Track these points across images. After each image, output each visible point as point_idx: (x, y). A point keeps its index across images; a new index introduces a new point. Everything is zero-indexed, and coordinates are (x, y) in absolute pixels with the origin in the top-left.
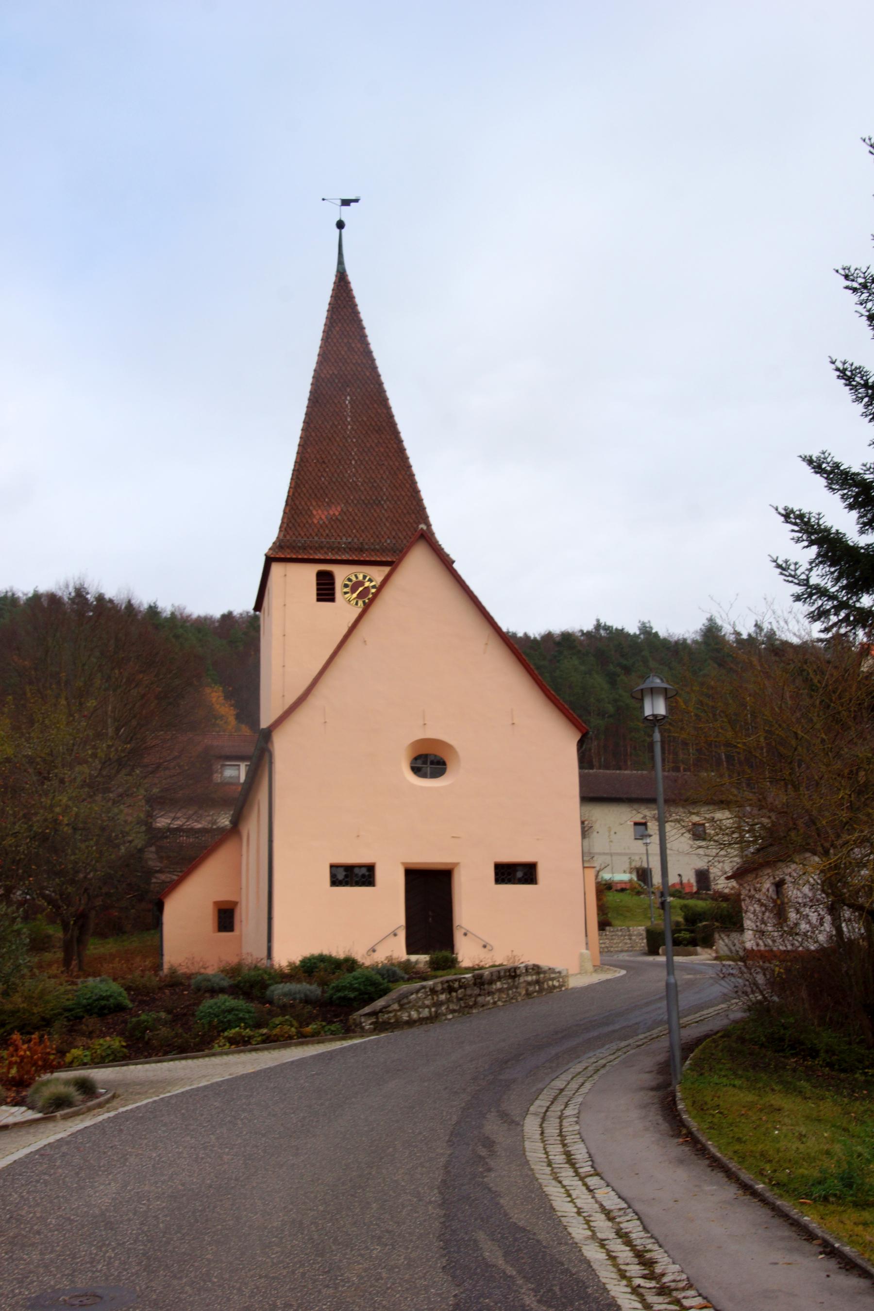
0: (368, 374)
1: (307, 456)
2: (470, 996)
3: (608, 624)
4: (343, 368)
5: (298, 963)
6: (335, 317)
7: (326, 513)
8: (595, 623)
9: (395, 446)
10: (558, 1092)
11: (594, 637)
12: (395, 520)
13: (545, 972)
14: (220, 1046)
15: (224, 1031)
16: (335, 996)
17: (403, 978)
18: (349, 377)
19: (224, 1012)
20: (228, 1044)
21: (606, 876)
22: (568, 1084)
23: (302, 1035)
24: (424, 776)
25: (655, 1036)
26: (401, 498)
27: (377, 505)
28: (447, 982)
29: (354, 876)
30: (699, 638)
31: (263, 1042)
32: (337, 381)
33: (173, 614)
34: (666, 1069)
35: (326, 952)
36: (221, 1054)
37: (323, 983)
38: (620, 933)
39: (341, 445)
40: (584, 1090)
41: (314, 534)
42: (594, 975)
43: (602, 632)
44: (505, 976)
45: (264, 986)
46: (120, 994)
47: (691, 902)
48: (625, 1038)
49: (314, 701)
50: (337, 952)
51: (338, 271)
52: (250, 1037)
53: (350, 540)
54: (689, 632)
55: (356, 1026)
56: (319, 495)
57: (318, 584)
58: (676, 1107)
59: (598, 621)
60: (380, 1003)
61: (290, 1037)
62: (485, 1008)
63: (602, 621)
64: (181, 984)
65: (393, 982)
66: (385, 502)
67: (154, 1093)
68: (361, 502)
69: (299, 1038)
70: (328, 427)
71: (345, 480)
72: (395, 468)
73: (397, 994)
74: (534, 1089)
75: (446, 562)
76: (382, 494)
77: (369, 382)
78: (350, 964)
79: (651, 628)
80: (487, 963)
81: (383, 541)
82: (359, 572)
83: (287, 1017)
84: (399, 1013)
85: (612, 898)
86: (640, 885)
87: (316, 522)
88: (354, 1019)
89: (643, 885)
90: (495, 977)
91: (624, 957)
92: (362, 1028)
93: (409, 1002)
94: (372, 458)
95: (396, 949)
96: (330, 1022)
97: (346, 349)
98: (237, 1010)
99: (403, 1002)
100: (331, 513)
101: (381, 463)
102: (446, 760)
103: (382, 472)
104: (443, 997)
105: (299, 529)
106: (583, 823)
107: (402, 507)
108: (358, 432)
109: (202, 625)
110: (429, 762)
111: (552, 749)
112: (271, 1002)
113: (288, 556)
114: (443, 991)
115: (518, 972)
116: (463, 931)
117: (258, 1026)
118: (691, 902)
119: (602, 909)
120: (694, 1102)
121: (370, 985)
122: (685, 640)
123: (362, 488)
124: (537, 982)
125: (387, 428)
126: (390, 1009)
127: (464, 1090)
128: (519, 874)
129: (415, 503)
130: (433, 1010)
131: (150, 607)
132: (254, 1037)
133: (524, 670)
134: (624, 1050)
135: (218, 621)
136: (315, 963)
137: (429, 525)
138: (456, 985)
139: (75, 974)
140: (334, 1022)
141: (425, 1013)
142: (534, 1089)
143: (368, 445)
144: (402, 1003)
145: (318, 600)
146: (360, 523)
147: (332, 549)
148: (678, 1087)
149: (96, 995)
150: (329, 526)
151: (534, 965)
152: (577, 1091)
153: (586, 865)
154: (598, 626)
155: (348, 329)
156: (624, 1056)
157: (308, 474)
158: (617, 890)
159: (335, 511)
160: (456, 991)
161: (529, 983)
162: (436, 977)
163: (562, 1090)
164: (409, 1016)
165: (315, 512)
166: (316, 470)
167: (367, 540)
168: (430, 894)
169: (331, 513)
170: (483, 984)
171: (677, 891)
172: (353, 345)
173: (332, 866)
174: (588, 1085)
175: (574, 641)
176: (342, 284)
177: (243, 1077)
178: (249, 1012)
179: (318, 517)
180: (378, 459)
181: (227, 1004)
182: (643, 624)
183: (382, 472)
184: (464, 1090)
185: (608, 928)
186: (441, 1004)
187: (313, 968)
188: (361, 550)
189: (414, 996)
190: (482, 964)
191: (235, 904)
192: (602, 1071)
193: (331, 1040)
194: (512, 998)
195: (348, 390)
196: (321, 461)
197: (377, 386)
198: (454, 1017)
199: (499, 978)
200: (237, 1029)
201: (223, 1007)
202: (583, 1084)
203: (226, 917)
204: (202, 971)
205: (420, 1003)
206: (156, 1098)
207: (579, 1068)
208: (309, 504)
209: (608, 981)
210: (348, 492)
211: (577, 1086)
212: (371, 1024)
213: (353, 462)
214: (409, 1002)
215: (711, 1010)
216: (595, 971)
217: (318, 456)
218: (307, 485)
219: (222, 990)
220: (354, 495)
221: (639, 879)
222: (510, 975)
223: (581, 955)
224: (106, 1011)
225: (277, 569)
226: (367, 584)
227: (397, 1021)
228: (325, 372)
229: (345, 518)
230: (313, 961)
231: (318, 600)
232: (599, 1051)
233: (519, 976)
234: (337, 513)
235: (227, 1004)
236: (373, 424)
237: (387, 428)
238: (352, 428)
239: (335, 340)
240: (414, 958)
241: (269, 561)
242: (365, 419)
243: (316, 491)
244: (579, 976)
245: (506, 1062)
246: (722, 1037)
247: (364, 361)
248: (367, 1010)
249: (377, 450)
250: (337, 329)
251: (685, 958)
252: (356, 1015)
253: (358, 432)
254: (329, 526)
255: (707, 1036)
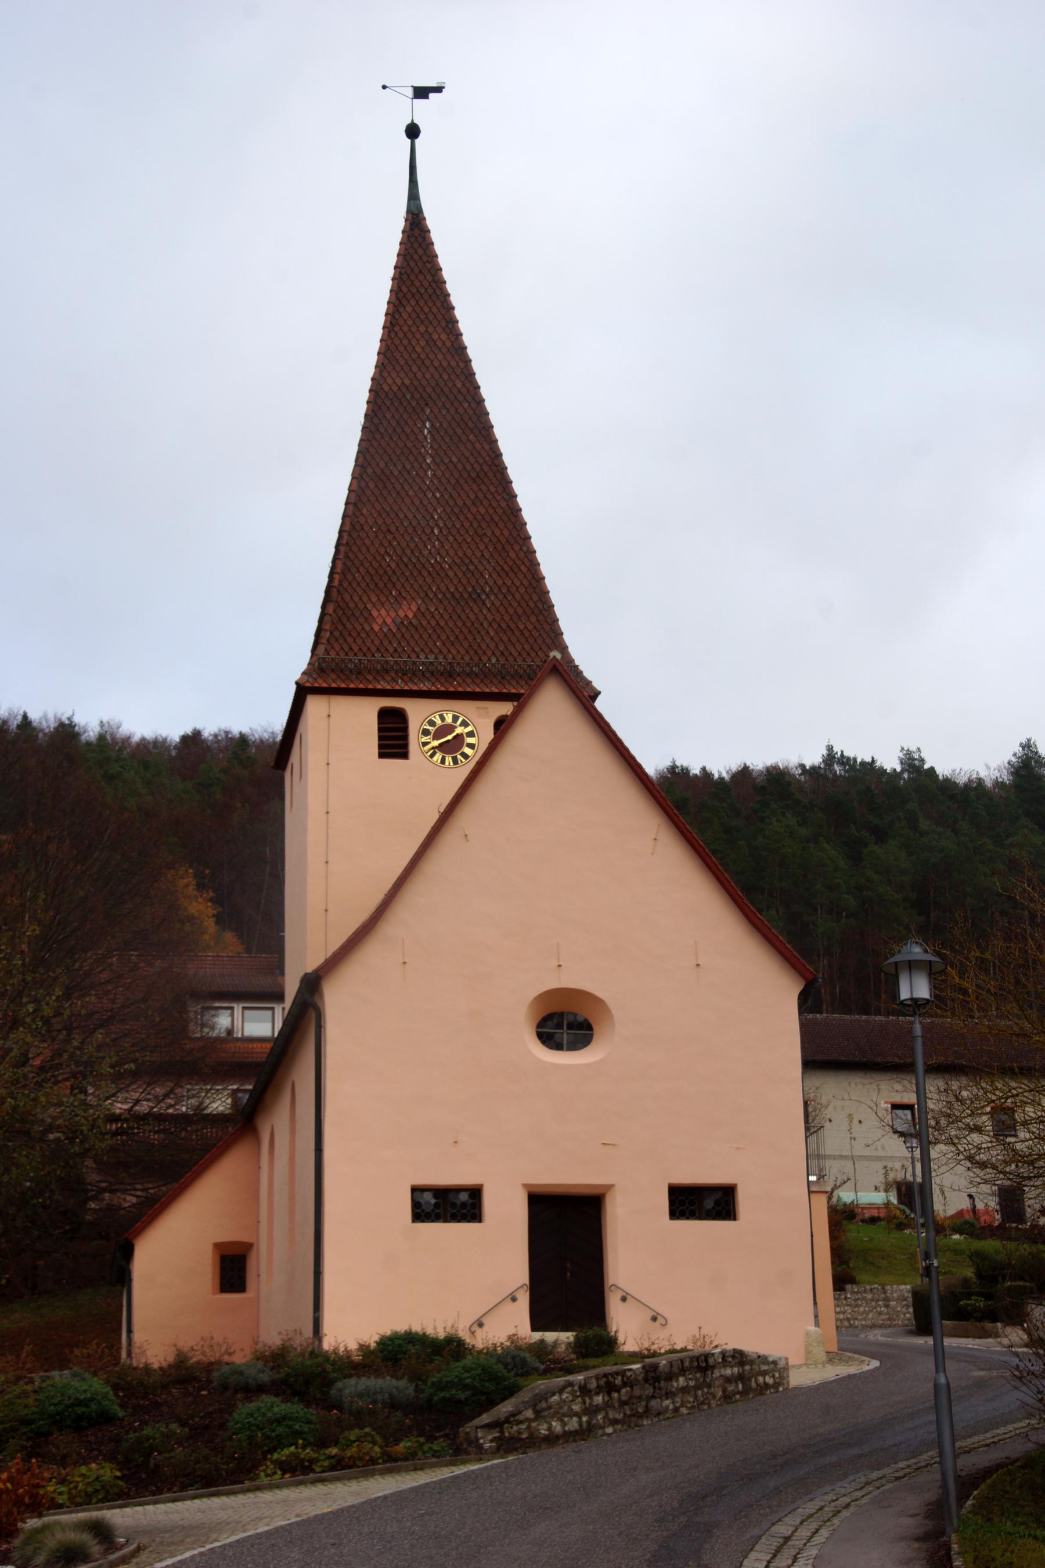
0: (459, 385)
1: (362, 520)
2: (640, 1398)
3: (849, 753)
4: (419, 375)
5: (373, 1345)
6: (404, 289)
7: (393, 614)
8: (825, 752)
9: (504, 504)
10: (781, 1541)
11: (824, 777)
12: (504, 626)
13: (751, 1362)
14: (267, 1475)
15: (272, 1450)
16: (427, 1397)
17: (537, 1369)
18: (429, 390)
19: (271, 1421)
20: (279, 1472)
21: (846, 1196)
22: (796, 1530)
23: (391, 1458)
24: (558, 1047)
25: (923, 1464)
26: (513, 589)
27: (475, 601)
28: (605, 1375)
29: (449, 1204)
30: (1006, 777)
31: (333, 1468)
32: (408, 397)
33: (101, 737)
34: (937, 1511)
35: (417, 1328)
36: (270, 1487)
37: (416, 1377)
38: (870, 1296)
39: (417, 503)
40: (818, 1539)
41: (373, 649)
42: (829, 1367)
43: (837, 768)
44: (691, 1368)
45: (328, 1383)
46: (105, 1396)
47: (990, 1245)
48: (878, 1466)
49: (390, 928)
50: (435, 1328)
51: (409, 211)
52: (312, 1461)
53: (431, 658)
54: (988, 767)
55: (470, 1443)
56: (381, 585)
57: (380, 730)
58: (951, 1564)
59: (830, 748)
60: (506, 1408)
61: (373, 1461)
62: (661, 1417)
63: (837, 749)
64: (195, 1379)
65: (521, 1375)
66: (487, 595)
67: (194, 1542)
68: (448, 596)
69: (385, 1462)
70: (396, 473)
71: (423, 560)
72: (503, 541)
73: (530, 1395)
74: (748, 1536)
75: (584, 695)
76: (482, 582)
77: (460, 398)
78: (452, 1348)
79: (922, 761)
80: (662, 1345)
81: (484, 659)
82: (445, 712)
83: (367, 1430)
84: (534, 1424)
85: (854, 1233)
86: (904, 1212)
87: (376, 628)
88: (467, 1434)
89: (908, 1211)
90: (675, 1370)
91: (877, 1336)
92: (480, 1447)
93: (550, 1407)
94: (467, 524)
95: (510, 1324)
96: (431, 1438)
97: (423, 343)
98: (291, 1419)
99: (539, 1406)
100: (402, 614)
101: (480, 532)
102: (591, 1022)
103: (482, 547)
104: (599, 1399)
105: (350, 640)
106: (806, 1104)
107: (515, 605)
108: (444, 481)
109: (149, 754)
110: (565, 1023)
111: (759, 1000)
112: (339, 1407)
113: (334, 685)
114: (599, 1390)
115: (711, 1361)
116: (620, 1294)
117: (322, 1443)
118: (990, 1245)
119: (839, 1254)
120: (976, 1558)
121: (490, 1380)
122: (980, 781)
123: (451, 574)
124: (741, 1377)
125: (490, 475)
126: (521, 1417)
127: (647, 1536)
128: (709, 1204)
129: (535, 598)
130: (584, 1419)
131: (62, 725)
132: (318, 1460)
133: (719, 885)
134: (877, 1484)
135: (175, 747)
136: (400, 1346)
137: (564, 649)
138: (618, 1381)
139: (28, 1365)
140: (437, 1438)
141: (573, 1424)
142: (748, 1536)
143: (460, 503)
144: (538, 1408)
145: (381, 755)
146: (448, 631)
147: (403, 673)
148: (954, 1538)
149: (70, 1398)
150: (399, 636)
151: (735, 1350)
152: (809, 1541)
153: (813, 1188)
154: (830, 757)
155: (426, 310)
156: (876, 1493)
157: (364, 550)
158: (862, 1221)
159: (408, 611)
160: (618, 1391)
161: (728, 1380)
162: (587, 1368)
163: (787, 1539)
164: (549, 1429)
165: (375, 613)
166: (377, 543)
167: (458, 657)
168: (567, 1231)
169: (402, 614)
170: (657, 1379)
171: (966, 1222)
172: (435, 337)
173: (415, 1190)
174: (824, 1533)
175: (789, 784)
176: (417, 232)
177: (320, 1519)
178: (309, 1422)
179: (380, 621)
180: (475, 525)
181: (276, 1409)
182: (909, 753)
183: (482, 547)
184: (647, 1536)
185: (848, 1287)
186: (597, 1409)
187: (400, 1352)
188: (450, 675)
189: (556, 1398)
190: (654, 1347)
191: (248, 1246)
192: (845, 1513)
193: (432, 1466)
194: (703, 1403)
195: (428, 411)
196: (384, 528)
197: (474, 405)
198: (615, 1431)
199: (683, 1371)
200: (293, 1448)
201: (270, 1414)
202: (817, 1531)
203: (233, 1268)
204: (226, 1358)
205: (565, 1409)
206: (202, 1550)
207: (810, 1508)
208: (365, 600)
209: (850, 1377)
210: (429, 580)
211: (809, 1534)
212: (491, 1441)
213: (436, 531)
214: (550, 1407)
215: (1010, 1427)
216: (830, 1361)
217: (380, 522)
218: (361, 569)
219: (261, 1389)
220: (437, 576)
221: (900, 1201)
222: (699, 1366)
223: (807, 1333)
224: (84, 1423)
225: (314, 705)
226: (459, 730)
227: (531, 1436)
228: (390, 381)
229: (424, 623)
230: (397, 1342)
231: (381, 755)
232: (839, 1484)
233: (713, 1367)
234: (411, 615)
235: (276, 1409)
236: (468, 467)
237: (490, 475)
238: (434, 475)
239: (405, 329)
240: (537, 1336)
241: (302, 693)
242: (455, 460)
243: (376, 579)
244: (804, 1369)
245: (703, 1498)
246: (1022, 1467)
247: (453, 364)
248: (485, 1418)
249: (474, 510)
250: (409, 309)
251: (978, 1341)
252: (468, 1427)
253: (444, 481)
254: (399, 636)
255: (999, 1466)
